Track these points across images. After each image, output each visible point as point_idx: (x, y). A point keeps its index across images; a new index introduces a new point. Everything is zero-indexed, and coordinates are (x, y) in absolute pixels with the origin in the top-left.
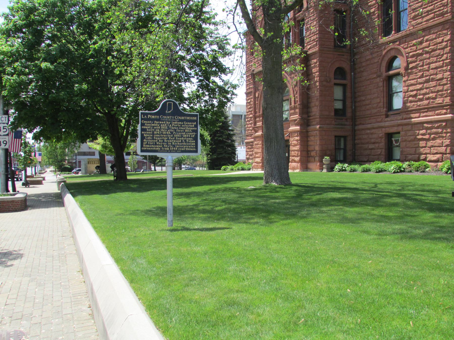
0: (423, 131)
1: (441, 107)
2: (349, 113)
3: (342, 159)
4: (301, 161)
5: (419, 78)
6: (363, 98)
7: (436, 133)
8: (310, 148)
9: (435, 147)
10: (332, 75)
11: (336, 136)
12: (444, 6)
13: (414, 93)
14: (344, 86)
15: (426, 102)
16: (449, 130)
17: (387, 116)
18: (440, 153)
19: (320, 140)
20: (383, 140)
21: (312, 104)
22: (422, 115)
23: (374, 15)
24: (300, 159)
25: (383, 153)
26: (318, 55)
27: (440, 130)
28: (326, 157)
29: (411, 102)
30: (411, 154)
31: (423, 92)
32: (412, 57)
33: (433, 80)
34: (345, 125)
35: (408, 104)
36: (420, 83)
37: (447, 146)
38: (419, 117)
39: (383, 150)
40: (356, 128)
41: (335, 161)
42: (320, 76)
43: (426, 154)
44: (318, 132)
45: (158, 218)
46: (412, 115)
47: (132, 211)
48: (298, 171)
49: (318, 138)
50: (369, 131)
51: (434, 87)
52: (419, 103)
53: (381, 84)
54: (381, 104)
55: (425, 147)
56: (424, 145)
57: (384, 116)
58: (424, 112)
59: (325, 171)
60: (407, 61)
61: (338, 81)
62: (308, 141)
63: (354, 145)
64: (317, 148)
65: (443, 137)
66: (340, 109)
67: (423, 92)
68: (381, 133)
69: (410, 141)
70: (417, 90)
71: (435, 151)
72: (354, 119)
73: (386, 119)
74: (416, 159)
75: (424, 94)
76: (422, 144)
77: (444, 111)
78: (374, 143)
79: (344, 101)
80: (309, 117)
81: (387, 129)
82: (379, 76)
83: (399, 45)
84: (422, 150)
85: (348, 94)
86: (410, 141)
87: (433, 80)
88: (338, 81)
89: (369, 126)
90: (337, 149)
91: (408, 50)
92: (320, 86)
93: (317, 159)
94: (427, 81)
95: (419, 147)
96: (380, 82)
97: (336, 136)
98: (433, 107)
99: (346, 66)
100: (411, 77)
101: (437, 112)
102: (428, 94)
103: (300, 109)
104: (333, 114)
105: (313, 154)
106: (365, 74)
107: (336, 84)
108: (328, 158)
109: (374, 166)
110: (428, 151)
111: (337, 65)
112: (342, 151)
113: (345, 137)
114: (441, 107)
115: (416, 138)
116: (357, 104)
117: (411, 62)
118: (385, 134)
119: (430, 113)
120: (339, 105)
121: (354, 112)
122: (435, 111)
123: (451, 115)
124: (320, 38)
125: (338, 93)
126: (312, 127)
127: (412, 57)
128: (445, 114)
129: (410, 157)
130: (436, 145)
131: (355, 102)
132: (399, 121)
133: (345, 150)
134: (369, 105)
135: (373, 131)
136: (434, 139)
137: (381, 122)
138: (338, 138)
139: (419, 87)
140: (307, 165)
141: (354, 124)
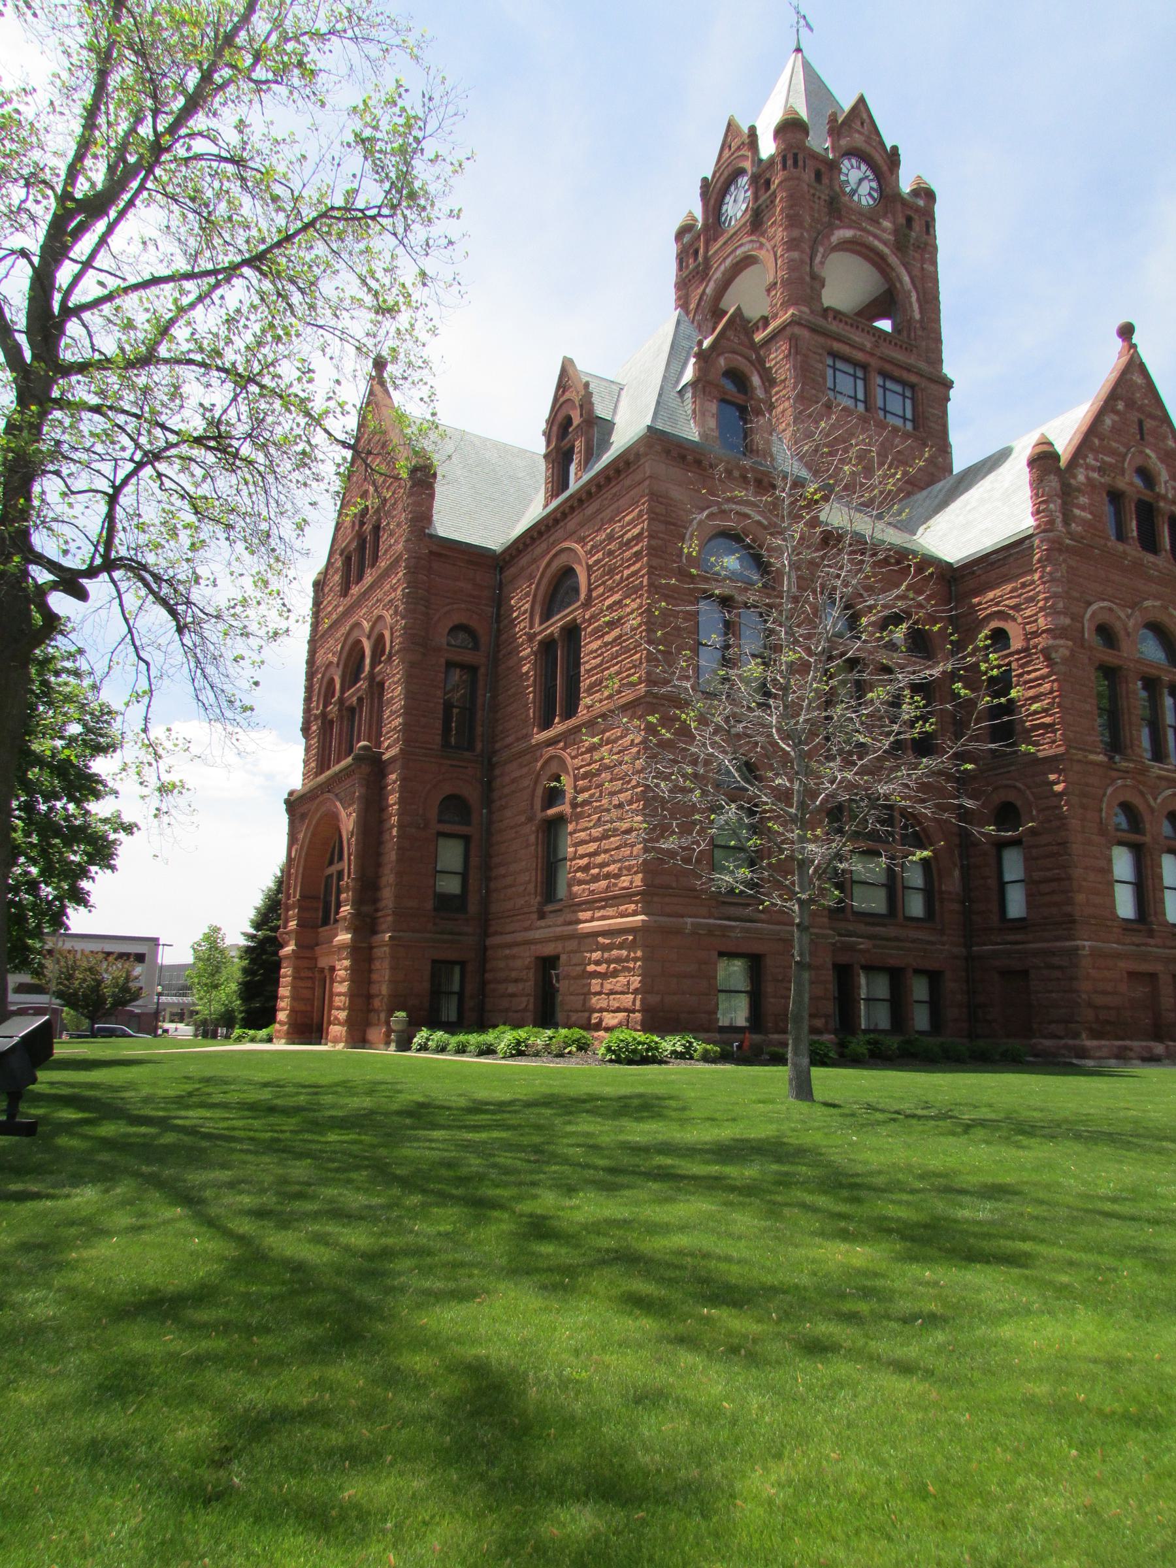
0: (596, 955)
1: (627, 897)
2: (473, 907)
3: (453, 1017)
4: (350, 1022)
5: (594, 826)
6: (502, 871)
7: (618, 960)
8: (374, 989)
9: (616, 993)
10: (433, 814)
11: (434, 962)
12: (634, 667)
13: (585, 861)
14: (466, 839)
15: (603, 884)
16: (639, 954)
17: (542, 915)
18: (626, 1010)
19: (392, 968)
20: (531, 974)
21: (384, 881)
22: (598, 914)
23: (528, 679)
24: (349, 1016)
25: (531, 1007)
26: (398, 764)
27: (624, 953)
28: (398, 1014)
29: (581, 882)
30: (577, 1011)
31: (599, 859)
32: (585, 776)
33: (615, 832)
34: (459, 934)
35: (575, 889)
36: (595, 840)
37: (636, 992)
38: (592, 919)
39: (830, 986)
40: (491, 941)
41: (414, 1024)
42: (401, 813)
43: (601, 1010)
44: (386, 949)
45: (791, 1080)
46: (582, 915)
47: (474, 1101)
48: (340, 1046)
49: (386, 964)
50: (507, 952)
51: (617, 848)
52: (593, 886)
53: (532, 838)
54: (531, 887)
55: (600, 993)
56: (598, 989)
57: (535, 916)
58: (600, 908)
59: (393, 1046)
60: (575, 787)
61: (447, 828)
62: (370, 971)
63: (484, 984)
64: (384, 990)
65: (629, 969)
66: (455, 896)
67: (599, 859)
68: (525, 958)
69: (575, 978)
70: (590, 855)
71: (616, 1005)
72: (485, 923)
73: (542, 923)
74: (584, 1022)
75: (602, 865)
76: (595, 984)
77: (633, 906)
78: (516, 981)
79: (465, 876)
80: (377, 910)
81: (539, 946)
82: (530, 819)
83: (564, 749)
84: (594, 1000)
85: (474, 861)
86: (575, 978)
87: (615, 832)
88: (447, 828)
89: (508, 938)
90: (437, 992)
91: (578, 762)
92: (398, 837)
93: (383, 1016)
94: (605, 836)
95: (589, 993)
96: (530, 833)
97: (434, 962)
98: (615, 897)
99: (471, 793)
100: (584, 823)
101: (622, 908)
102: (608, 865)
103: (354, 890)
104: (429, 905)
105: (377, 1003)
106: (508, 813)
107: (441, 834)
108: (401, 1014)
109: (504, 1037)
110: (604, 1004)
111: (447, 789)
112: (454, 1000)
113: (462, 964)
114: (627, 897)
115: (584, 971)
116: (492, 885)
117: (583, 790)
118: (537, 958)
119: (610, 911)
120: (451, 885)
121: (486, 902)
122: (618, 905)
123: (642, 917)
124: (404, 724)
125: (450, 855)
126: (378, 937)
127: (585, 776)
128: (635, 913)
129: (574, 1017)
130: (618, 988)
131: (489, 879)
132: (559, 929)
133: (461, 995)
134: (511, 886)
135: (515, 951)
136: (615, 974)
137: (526, 929)
138: (440, 968)
139: (592, 847)
140: (364, 1033)
141: (486, 934)
